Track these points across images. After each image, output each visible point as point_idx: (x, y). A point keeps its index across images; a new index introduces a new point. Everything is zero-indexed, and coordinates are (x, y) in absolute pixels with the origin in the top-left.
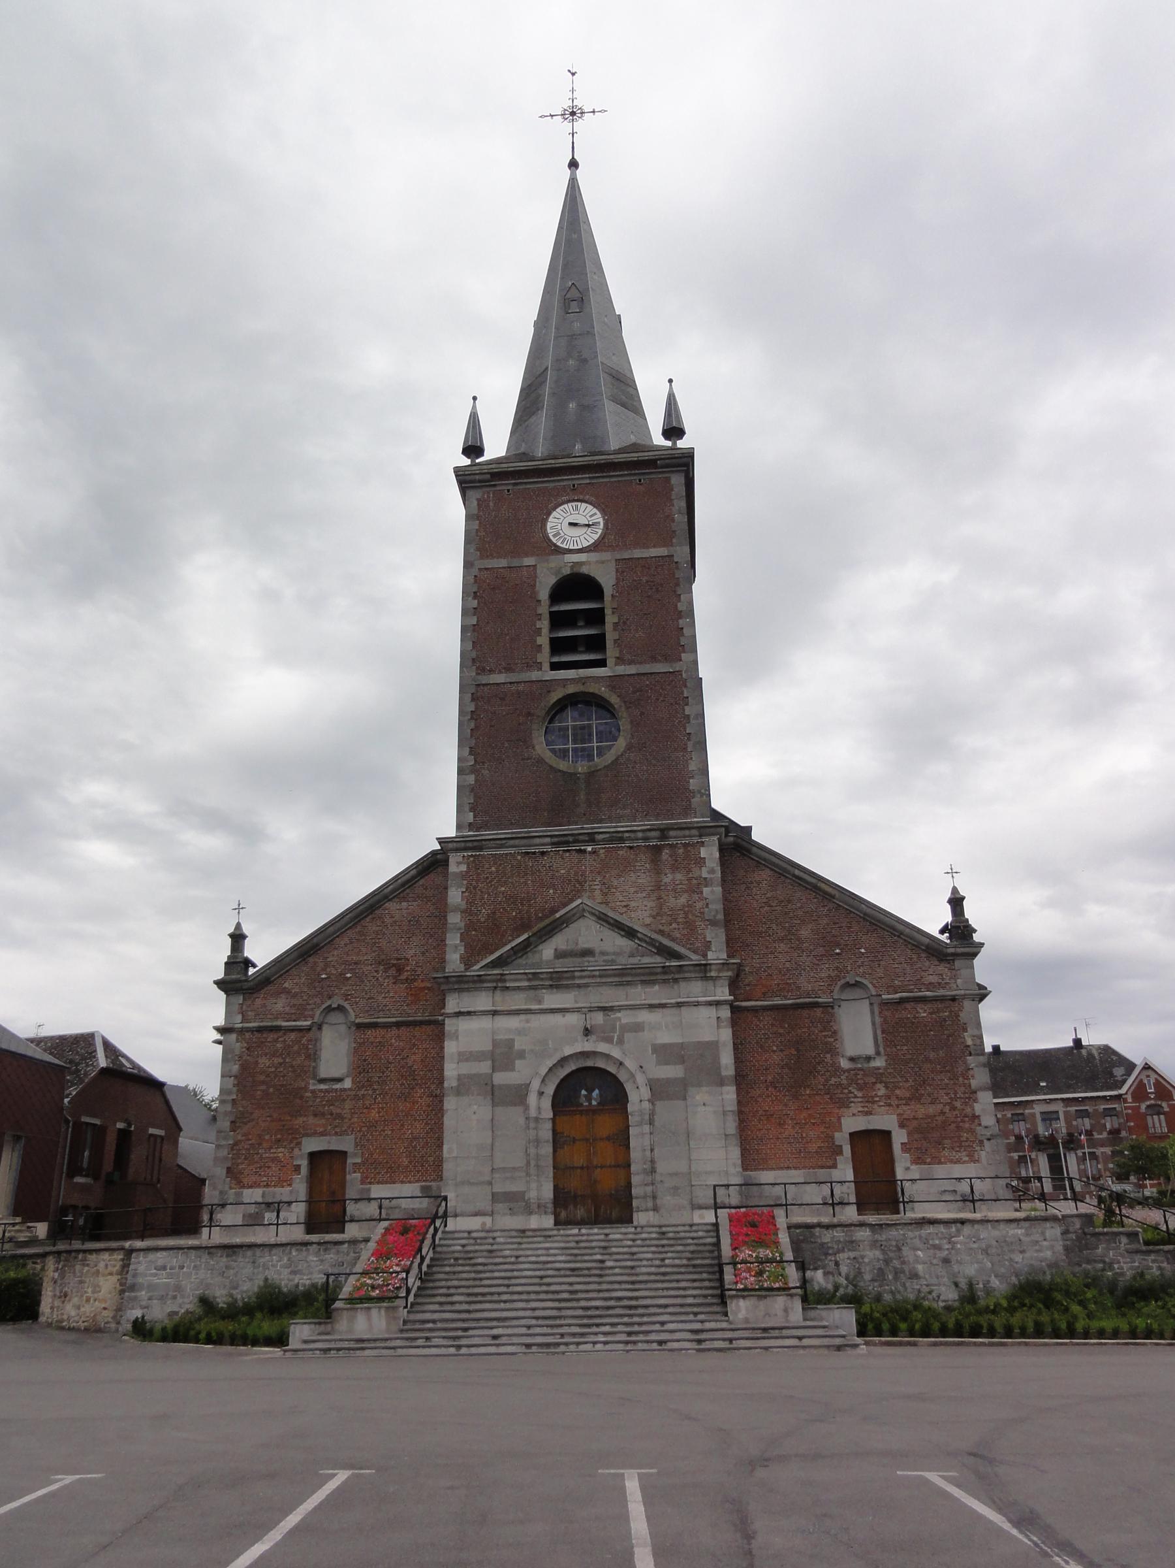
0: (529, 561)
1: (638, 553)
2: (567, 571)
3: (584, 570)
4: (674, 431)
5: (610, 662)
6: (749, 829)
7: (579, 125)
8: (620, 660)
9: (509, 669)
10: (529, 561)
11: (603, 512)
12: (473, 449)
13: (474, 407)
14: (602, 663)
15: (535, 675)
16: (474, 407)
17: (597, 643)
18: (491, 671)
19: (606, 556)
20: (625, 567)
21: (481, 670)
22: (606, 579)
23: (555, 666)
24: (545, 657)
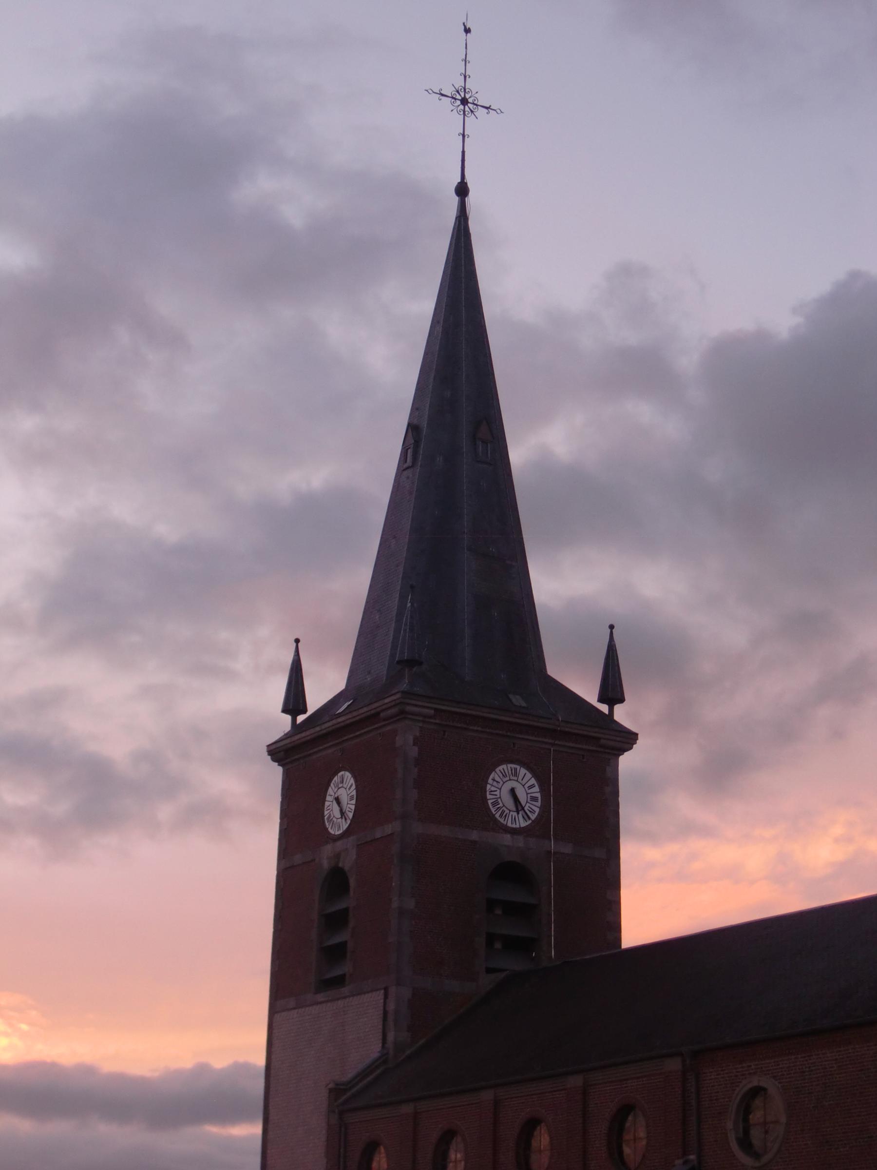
11: (356, 782)
12: (295, 700)
13: (611, 633)
16: (611, 633)
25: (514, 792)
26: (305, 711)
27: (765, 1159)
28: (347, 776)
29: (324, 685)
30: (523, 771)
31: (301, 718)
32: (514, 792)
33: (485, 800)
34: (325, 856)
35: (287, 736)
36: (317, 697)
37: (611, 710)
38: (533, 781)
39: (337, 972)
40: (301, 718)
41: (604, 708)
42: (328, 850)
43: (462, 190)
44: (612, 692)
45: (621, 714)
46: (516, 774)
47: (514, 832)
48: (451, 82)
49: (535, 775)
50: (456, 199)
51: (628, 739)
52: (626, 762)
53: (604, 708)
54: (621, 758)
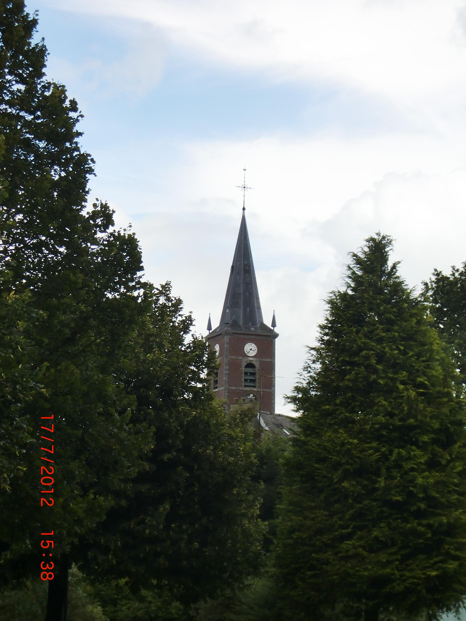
0: (240, 358)
1: (264, 360)
2: (249, 362)
3: (252, 362)
4: (274, 325)
5: (257, 387)
6: (26, 6)
7: (248, 192)
8: (259, 387)
9: (235, 386)
10: (240, 358)
11: (257, 348)
12: (209, 328)
13: (244, 213)
14: (254, 387)
15: (241, 388)
16: (244, 213)
17: (254, 381)
18: (232, 386)
19: (257, 359)
20: (261, 363)
21: (229, 385)
22: (257, 364)
23: (245, 386)
24: (243, 384)
25: (251, 349)
26: (211, 329)
28: (218, 345)
29: (216, 324)
31: (211, 331)
32: (251, 349)
35: (208, 335)
36: (214, 328)
39: (216, 386)
40: (211, 331)
41: (272, 328)
43: (244, 209)
45: (276, 330)
47: (252, 357)
48: (241, 184)
52: (277, 340)
53: (272, 328)
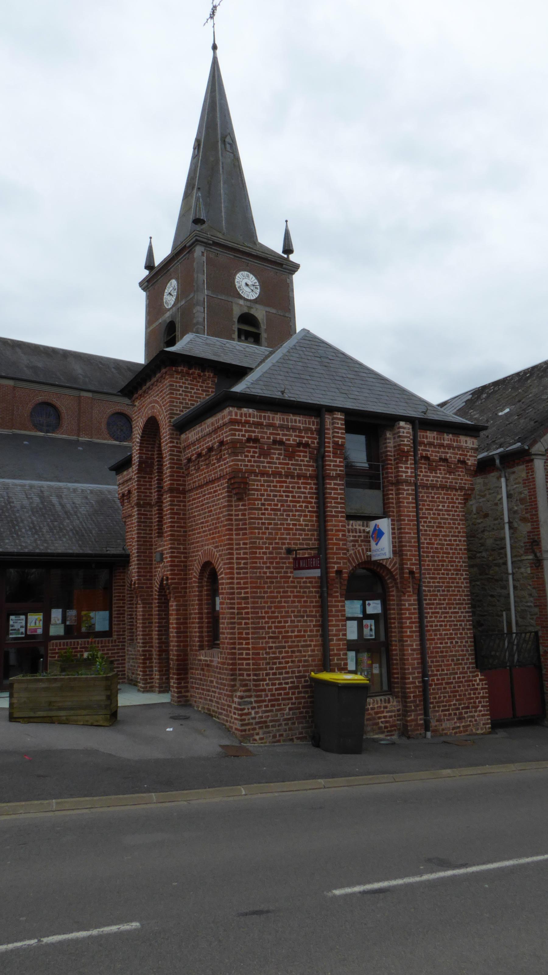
13: (287, 226)
25: (247, 284)
27: (136, 459)
30: (251, 276)
33: (235, 286)
34: (167, 316)
37: (288, 257)
38: (256, 281)
41: (286, 256)
42: (168, 314)
43: (215, 47)
44: (288, 250)
45: (293, 258)
46: (248, 276)
49: (256, 299)
50: (212, 51)
51: (295, 267)
52: (297, 278)
53: (286, 256)
54: (294, 276)
